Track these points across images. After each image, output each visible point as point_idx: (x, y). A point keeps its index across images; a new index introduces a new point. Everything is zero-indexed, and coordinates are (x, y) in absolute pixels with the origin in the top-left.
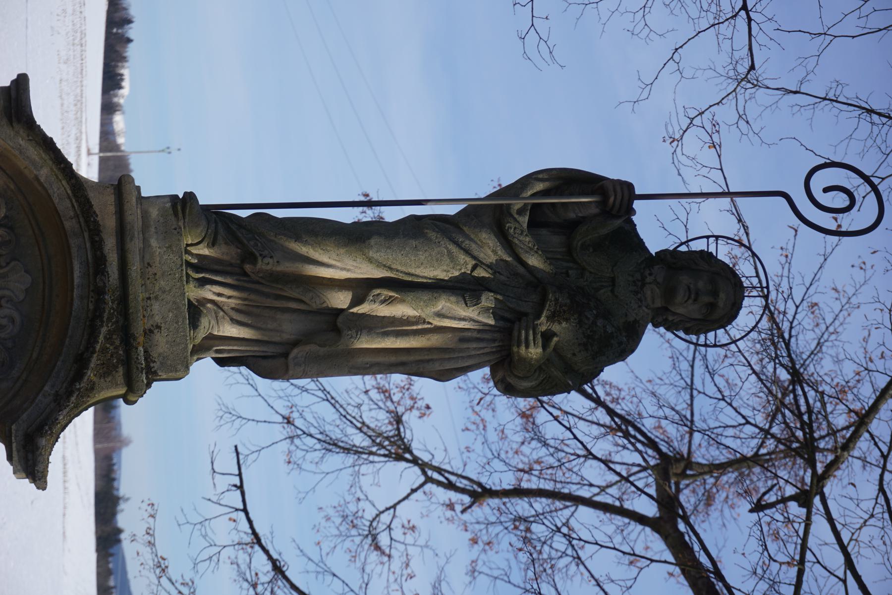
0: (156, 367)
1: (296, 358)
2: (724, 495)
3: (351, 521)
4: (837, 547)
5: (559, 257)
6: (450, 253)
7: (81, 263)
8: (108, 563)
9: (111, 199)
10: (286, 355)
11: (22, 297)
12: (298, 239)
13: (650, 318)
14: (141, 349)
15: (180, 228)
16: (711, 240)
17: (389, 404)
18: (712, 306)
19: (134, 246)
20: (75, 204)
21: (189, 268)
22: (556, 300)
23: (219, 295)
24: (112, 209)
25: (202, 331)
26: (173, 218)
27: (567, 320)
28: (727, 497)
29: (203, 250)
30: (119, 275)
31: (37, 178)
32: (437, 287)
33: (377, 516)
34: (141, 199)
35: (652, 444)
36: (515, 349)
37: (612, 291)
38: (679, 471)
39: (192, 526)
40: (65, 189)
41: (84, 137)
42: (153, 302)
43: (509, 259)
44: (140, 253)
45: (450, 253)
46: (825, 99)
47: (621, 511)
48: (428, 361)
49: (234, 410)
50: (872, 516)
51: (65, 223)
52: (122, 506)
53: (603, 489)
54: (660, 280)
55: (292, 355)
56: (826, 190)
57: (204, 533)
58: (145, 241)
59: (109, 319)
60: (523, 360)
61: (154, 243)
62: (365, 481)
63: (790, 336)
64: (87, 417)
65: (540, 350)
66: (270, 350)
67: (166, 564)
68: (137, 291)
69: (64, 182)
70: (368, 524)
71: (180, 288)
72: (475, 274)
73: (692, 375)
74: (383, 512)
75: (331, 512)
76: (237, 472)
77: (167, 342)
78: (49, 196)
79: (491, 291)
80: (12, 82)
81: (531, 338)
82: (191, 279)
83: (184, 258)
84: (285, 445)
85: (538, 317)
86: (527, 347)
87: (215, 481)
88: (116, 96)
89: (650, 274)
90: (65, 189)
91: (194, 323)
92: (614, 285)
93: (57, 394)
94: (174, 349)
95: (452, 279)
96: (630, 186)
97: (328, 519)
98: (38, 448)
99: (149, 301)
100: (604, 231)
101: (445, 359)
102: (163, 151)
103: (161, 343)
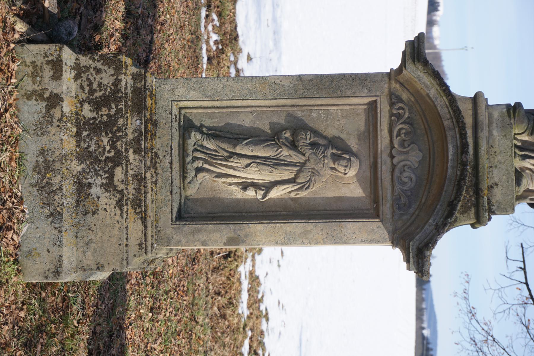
0: (494, 209)
7: (453, 147)
8: (422, 294)
9: (470, 106)
11: (416, 166)
14: (486, 198)
15: (512, 124)
19: (483, 135)
20: (451, 111)
21: (516, 149)
24: (470, 112)
25: (523, 187)
26: (508, 118)
29: (525, 138)
30: (473, 152)
31: (428, 95)
34: (488, 106)
39: (493, 291)
40: (445, 102)
42: (494, 169)
44: (486, 139)
49: (520, 220)
51: (444, 122)
57: (500, 295)
58: (490, 132)
61: (495, 133)
67: (475, 312)
68: (484, 161)
69: (444, 98)
71: (510, 161)
76: (522, 260)
77: (502, 194)
78: (435, 106)
80: (415, 37)
82: (517, 155)
83: (513, 142)
87: (508, 264)
88: (435, 15)
90: (445, 102)
91: (518, 182)
93: (437, 225)
94: (506, 198)
98: (425, 257)
99: (491, 168)
102: (463, 49)
103: (498, 194)
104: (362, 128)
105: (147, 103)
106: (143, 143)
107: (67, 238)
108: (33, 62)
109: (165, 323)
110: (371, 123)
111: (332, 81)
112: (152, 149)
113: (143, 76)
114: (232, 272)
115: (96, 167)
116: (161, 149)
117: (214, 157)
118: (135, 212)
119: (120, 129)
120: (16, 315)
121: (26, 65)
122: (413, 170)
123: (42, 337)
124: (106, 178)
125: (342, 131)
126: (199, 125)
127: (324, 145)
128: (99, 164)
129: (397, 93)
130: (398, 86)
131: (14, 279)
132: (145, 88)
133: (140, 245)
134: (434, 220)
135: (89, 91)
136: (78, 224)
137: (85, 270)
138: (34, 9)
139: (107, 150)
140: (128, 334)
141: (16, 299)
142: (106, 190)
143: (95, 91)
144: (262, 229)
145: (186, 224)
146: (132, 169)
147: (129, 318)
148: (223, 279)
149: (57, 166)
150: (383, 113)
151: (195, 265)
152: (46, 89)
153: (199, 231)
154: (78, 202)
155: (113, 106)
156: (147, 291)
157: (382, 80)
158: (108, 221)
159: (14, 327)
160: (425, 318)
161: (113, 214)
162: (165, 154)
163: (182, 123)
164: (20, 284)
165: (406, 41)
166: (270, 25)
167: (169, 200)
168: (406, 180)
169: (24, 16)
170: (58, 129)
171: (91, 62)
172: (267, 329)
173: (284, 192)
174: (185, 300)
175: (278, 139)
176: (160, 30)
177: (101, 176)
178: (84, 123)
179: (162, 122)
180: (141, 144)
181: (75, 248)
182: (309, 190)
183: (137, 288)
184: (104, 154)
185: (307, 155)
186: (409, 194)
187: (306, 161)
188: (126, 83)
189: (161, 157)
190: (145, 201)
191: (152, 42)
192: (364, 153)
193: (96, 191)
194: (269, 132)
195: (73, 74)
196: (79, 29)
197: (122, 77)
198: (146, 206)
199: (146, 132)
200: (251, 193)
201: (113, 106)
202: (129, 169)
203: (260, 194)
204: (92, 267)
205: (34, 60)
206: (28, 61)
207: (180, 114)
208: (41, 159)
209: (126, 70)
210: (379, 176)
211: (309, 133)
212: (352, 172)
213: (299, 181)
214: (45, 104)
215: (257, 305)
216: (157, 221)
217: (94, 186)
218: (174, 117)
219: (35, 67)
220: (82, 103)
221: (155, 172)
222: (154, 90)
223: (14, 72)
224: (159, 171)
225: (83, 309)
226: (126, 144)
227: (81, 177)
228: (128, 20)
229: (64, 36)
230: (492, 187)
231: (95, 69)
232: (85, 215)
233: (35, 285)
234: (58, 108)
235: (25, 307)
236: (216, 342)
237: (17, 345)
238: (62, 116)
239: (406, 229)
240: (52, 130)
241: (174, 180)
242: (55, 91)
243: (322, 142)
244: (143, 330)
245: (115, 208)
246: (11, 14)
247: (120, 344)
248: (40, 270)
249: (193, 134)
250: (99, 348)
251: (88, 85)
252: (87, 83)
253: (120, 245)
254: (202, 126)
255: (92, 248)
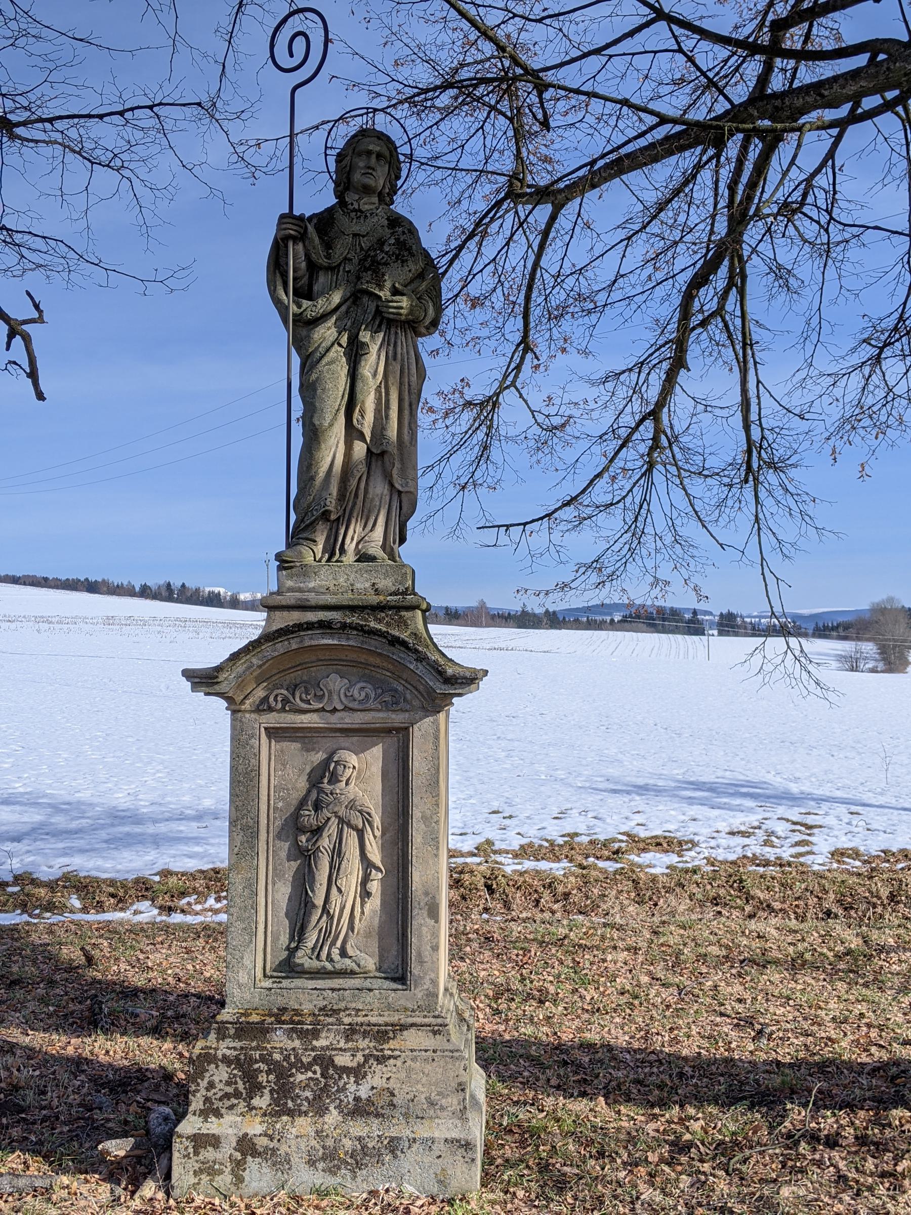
1: (402, 485)
2: (543, 147)
3: (541, 445)
4: (583, 61)
5: (335, 277)
6: (328, 364)
10: (400, 493)
11: (347, 681)
12: (312, 479)
13: (386, 207)
14: (388, 598)
16: (328, 152)
17: (457, 410)
18: (379, 156)
19: (313, 598)
22: (367, 282)
23: (352, 539)
26: (294, 570)
27: (383, 275)
28: (545, 145)
31: (260, 667)
32: (353, 375)
33: (538, 424)
35: (499, 204)
36: (403, 318)
37: (363, 236)
38: (519, 184)
41: (255, 623)
42: (355, 588)
43: (334, 318)
45: (328, 364)
46: (230, 42)
47: (546, 234)
48: (409, 385)
50: (560, 30)
52: (529, 609)
53: (530, 246)
54: (357, 197)
55: (400, 488)
56: (291, 55)
59: (366, 620)
60: (411, 312)
61: (312, 585)
62: (512, 432)
63: (416, 87)
64: (433, 629)
65: (405, 298)
66: (395, 504)
68: (346, 598)
69: (263, 647)
70: (544, 432)
72: (345, 345)
73: (446, 168)
74: (536, 420)
75: (535, 458)
77: (385, 579)
79: (358, 334)
81: (395, 304)
84: (479, 490)
85: (379, 297)
86: (401, 308)
89: (352, 204)
91: (373, 559)
92: (359, 235)
93: (416, 660)
95: (349, 364)
96: (282, 217)
97: (538, 462)
98: (454, 675)
100: (317, 240)
101: (409, 373)
104: (299, 745)
105: (256, 1020)
106: (305, 1027)
107: (423, 1131)
108: (195, 1173)
109: (562, 982)
110: (293, 735)
111: (239, 782)
112: (314, 1015)
113: (221, 1025)
114: (511, 883)
115: (333, 1090)
116: (315, 1002)
117: (328, 933)
118: (393, 1039)
119: (287, 1058)
120: (521, 1203)
121: (198, 1184)
122: (352, 685)
123: (554, 1165)
124: (348, 1078)
125: (302, 771)
126: (287, 952)
127: (318, 794)
128: (330, 1086)
129: (257, 703)
130: (247, 702)
131: (473, 1204)
132: (236, 1023)
133: (435, 1033)
134: (411, 663)
135: (236, 1098)
136: (406, 1116)
137: (465, 1108)
138: (127, 1170)
139: (312, 1076)
140: (566, 1037)
141: (500, 1203)
142: (364, 1077)
143: (236, 1089)
144: (418, 873)
145: (411, 972)
146: (338, 1041)
147: (547, 1035)
148: (518, 895)
149: (330, 1143)
150: (281, 721)
151: (493, 937)
152: (231, 1155)
153: (419, 955)
154: (377, 1115)
155: (256, 1066)
156: (517, 1008)
157: (241, 721)
158: (403, 1075)
159: (535, 1206)
160: (599, 618)
161: (394, 1069)
162: (321, 998)
163: (283, 974)
164: (481, 1197)
165: (193, 691)
166: (204, 825)
167: (380, 993)
168: (363, 694)
169: (135, 1184)
170: (283, 1140)
171: (198, 1095)
172: (588, 835)
173: (374, 844)
174: (535, 954)
175: (309, 850)
176: (186, 983)
177: (346, 1084)
178: (276, 1106)
179: (280, 1002)
180: (307, 1029)
181: (436, 1120)
182: (373, 813)
183: (511, 1023)
184: (317, 1079)
185: (329, 815)
186: (380, 691)
187: (336, 816)
188: (228, 1048)
189: (325, 1003)
190: (380, 1026)
191: (198, 996)
192: (329, 743)
193: (364, 1091)
194: (299, 862)
195: (214, 1119)
196: (164, 1103)
197: (219, 1054)
198: (387, 1025)
199: (292, 1022)
200: (375, 887)
201: (256, 1066)
202: (338, 1046)
203: (376, 876)
204: (462, 1098)
205: (191, 1173)
206: (193, 1180)
207: (272, 977)
208: (321, 1165)
209: (211, 1048)
210: (357, 726)
211: (302, 812)
212: (353, 759)
213: (360, 826)
214: (249, 1158)
215: (556, 848)
216: (406, 1009)
217: (358, 1094)
218: (275, 985)
219: (201, 1171)
220: (251, 1108)
221: (344, 1011)
222: (241, 1011)
223: (207, 1200)
224: (342, 1005)
225: (525, 1103)
226: (306, 1050)
227: (345, 1111)
228: (163, 1031)
229: (167, 1128)
230: (376, 590)
231: (208, 1089)
232: (394, 1106)
233: (486, 1173)
234: (256, 1140)
235: (511, 1190)
236: (599, 907)
237: (559, 1202)
238: (266, 1135)
239: (422, 695)
240: (283, 1149)
241: (354, 986)
242: (234, 1144)
243: (314, 795)
244: (566, 1015)
245: (386, 1066)
246: (130, 1204)
247: (579, 1049)
248: (464, 1169)
249: (297, 961)
250: (579, 1081)
251: (229, 1099)
252: (225, 1101)
253: (433, 1060)
254: (288, 948)
255: (437, 1097)
